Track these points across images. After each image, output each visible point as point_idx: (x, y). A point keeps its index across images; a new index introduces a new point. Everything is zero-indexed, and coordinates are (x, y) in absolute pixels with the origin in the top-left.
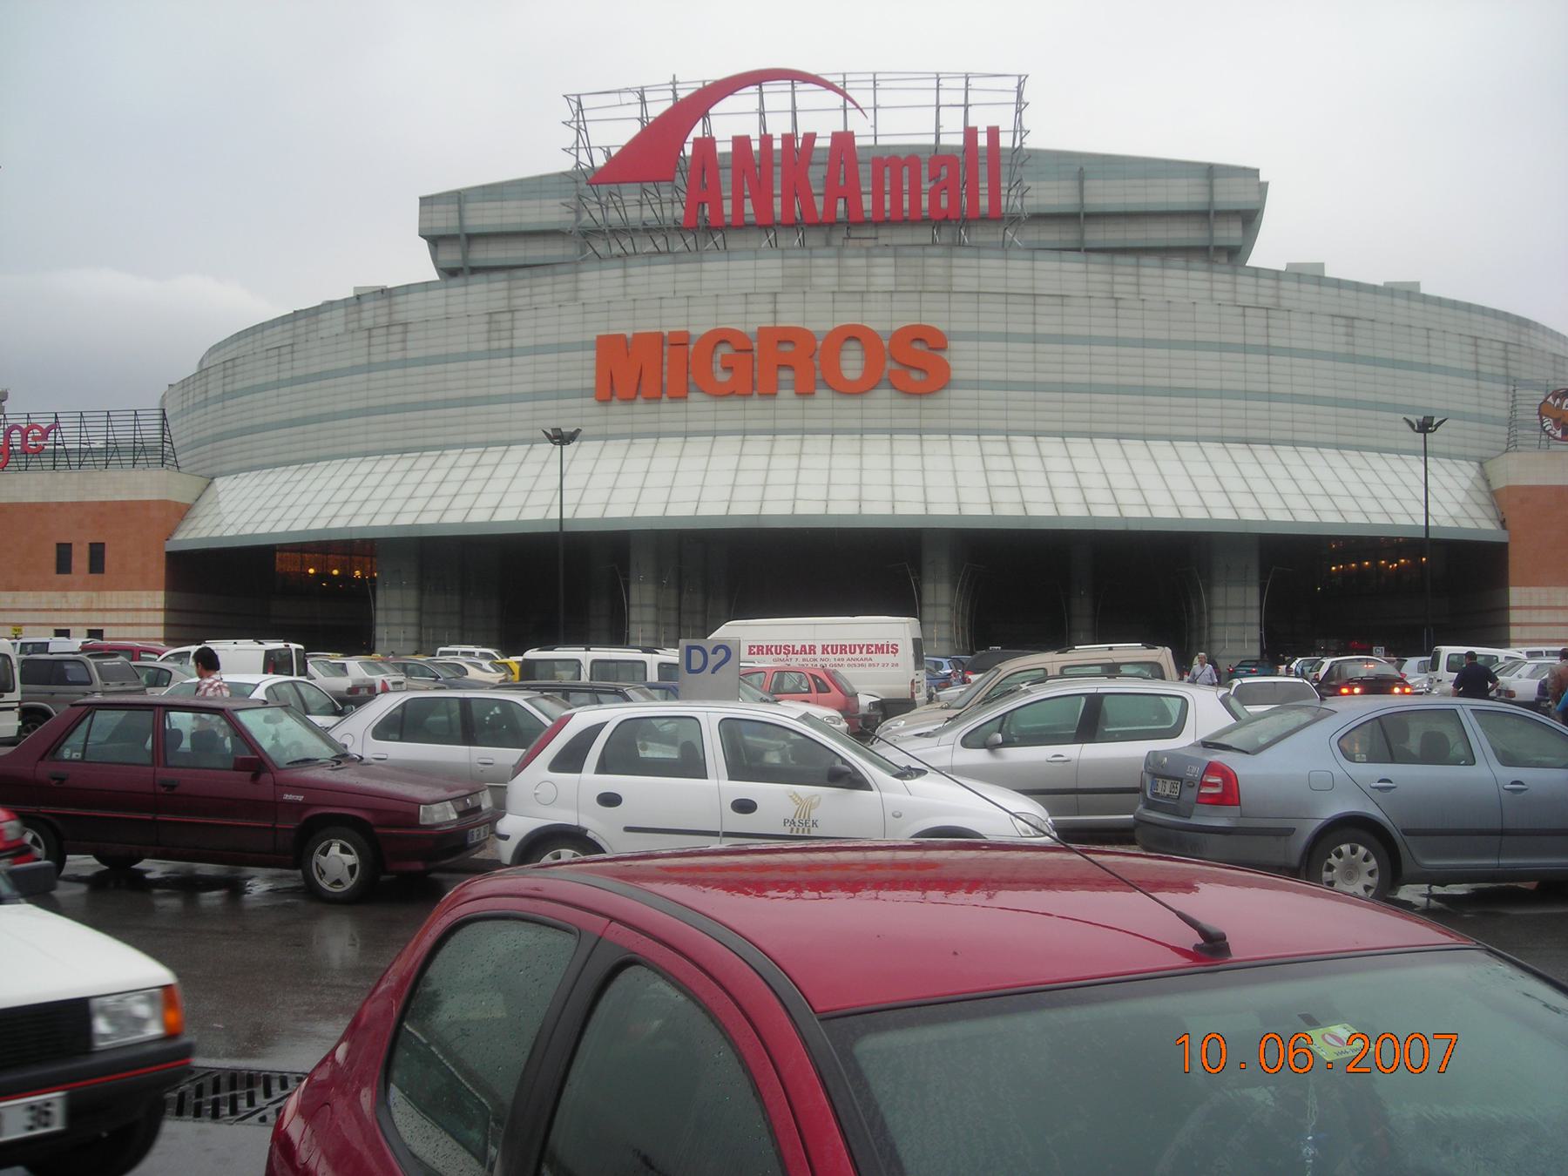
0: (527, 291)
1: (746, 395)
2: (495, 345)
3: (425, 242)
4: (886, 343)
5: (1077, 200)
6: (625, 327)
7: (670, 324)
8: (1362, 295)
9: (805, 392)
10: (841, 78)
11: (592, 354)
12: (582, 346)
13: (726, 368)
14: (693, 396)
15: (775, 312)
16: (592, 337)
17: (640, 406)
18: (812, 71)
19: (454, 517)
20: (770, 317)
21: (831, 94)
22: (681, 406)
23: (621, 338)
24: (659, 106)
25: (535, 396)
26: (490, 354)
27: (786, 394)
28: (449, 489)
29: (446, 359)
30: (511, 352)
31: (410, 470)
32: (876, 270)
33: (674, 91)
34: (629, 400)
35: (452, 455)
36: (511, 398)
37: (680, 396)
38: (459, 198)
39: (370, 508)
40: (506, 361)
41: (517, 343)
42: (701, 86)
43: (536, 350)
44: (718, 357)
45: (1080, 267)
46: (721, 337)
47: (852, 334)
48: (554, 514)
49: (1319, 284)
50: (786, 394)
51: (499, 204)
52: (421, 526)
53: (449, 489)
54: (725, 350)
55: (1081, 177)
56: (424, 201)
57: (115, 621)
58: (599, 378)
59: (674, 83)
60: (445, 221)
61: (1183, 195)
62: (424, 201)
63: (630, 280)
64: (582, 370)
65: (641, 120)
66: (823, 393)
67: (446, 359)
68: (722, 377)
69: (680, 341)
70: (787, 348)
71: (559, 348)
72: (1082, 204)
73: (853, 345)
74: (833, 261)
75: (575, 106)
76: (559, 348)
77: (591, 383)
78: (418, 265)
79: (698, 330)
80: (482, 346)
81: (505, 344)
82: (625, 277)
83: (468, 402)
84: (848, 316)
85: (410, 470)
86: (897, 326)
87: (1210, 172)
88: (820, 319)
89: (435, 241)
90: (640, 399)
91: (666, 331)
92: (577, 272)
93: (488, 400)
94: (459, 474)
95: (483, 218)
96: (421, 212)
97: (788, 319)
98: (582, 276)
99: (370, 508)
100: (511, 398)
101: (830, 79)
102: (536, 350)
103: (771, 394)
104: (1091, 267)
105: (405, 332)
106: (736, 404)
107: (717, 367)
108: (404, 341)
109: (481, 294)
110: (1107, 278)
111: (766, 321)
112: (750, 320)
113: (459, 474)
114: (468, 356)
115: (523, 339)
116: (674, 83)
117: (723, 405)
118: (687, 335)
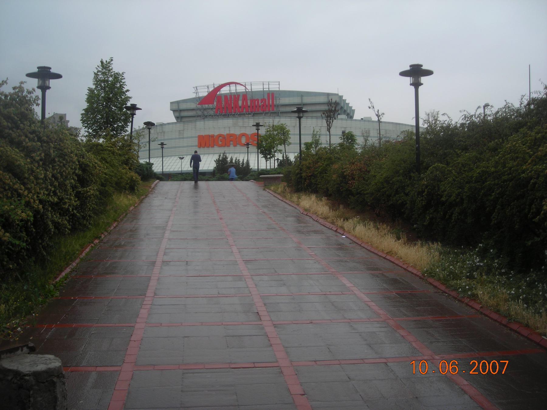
0: (187, 126)
1: (224, 146)
2: (180, 136)
3: (172, 112)
4: (250, 136)
5: (301, 101)
6: (203, 134)
7: (211, 133)
8: (357, 122)
9: (235, 145)
10: (244, 83)
11: (197, 139)
12: (195, 137)
13: (221, 141)
14: (215, 146)
15: (230, 131)
16: (197, 135)
17: (206, 148)
18: (238, 82)
19: (172, 170)
20: (229, 131)
21: (242, 86)
22: (213, 148)
23: (202, 136)
24: (211, 89)
25: (187, 146)
26: (179, 138)
27: (232, 146)
28: (171, 164)
29: (172, 139)
30: (183, 138)
31: (177, 160)
32: (250, 122)
33: (214, 86)
34: (204, 147)
35: (173, 157)
36: (183, 147)
37: (213, 147)
38: (178, 102)
39: (174, 167)
40: (182, 140)
41: (184, 136)
42: (218, 85)
43: (187, 138)
44: (219, 139)
45: (290, 119)
46: (220, 136)
47: (243, 135)
48: (180, 170)
49: (342, 120)
50: (232, 146)
51: (186, 104)
52: (175, 171)
53: (171, 164)
54: (221, 138)
55: (302, 96)
56: (171, 103)
57: (270, 366)
58: (198, 143)
59: (214, 84)
60: (175, 107)
61: (323, 99)
62: (171, 103)
63: (205, 124)
64: (195, 142)
65: (208, 92)
66: (238, 146)
67: (172, 139)
68: (220, 143)
69: (213, 136)
70: (232, 137)
71: (192, 137)
72: (302, 102)
73: (244, 137)
74: (242, 120)
75: (195, 89)
76: (192, 137)
77: (197, 144)
78: (171, 118)
79: (216, 134)
80: (178, 137)
81: (182, 136)
82: (204, 123)
83: (175, 147)
84: (243, 131)
85: (177, 160)
86: (252, 133)
87: (328, 95)
88: (237, 131)
89: (174, 111)
90: (206, 147)
91: (210, 134)
92: (196, 122)
93: (179, 147)
94: (174, 161)
95: (183, 106)
96: (170, 105)
97: (232, 132)
98: (197, 123)
99: (174, 167)
100: (183, 147)
101: (242, 84)
102: (187, 138)
103: (229, 146)
104: (292, 119)
105: (164, 134)
106: (223, 148)
107: (219, 141)
108: (164, 135)
109: (180, 126)
110: (295, 121)
111: (228, 132)
112: (225, 132)
113: (174, 161)
114: (176, 139)
115: (185, 136)
116: (214, 84)
117: (220, 148)
118: (214, 135)
